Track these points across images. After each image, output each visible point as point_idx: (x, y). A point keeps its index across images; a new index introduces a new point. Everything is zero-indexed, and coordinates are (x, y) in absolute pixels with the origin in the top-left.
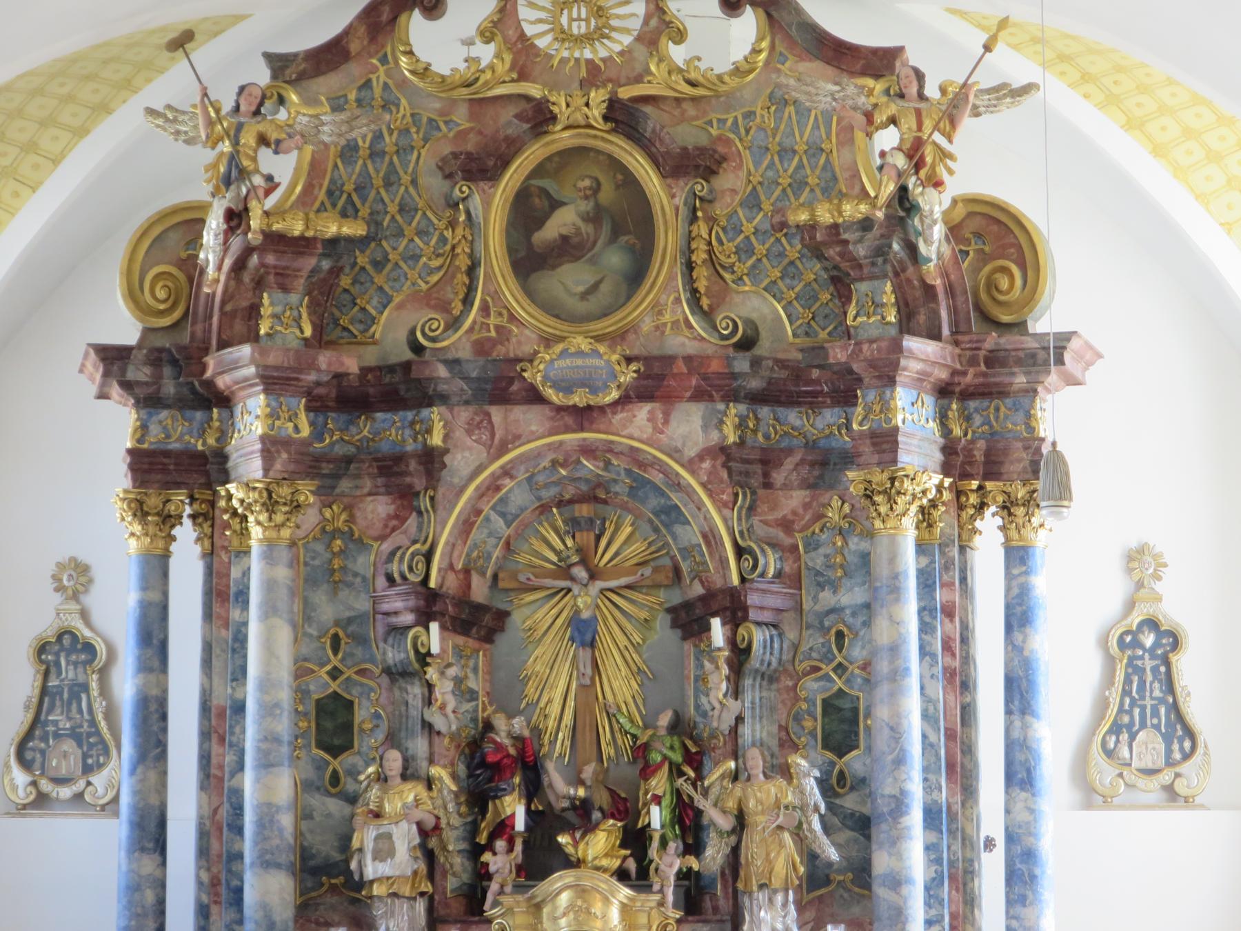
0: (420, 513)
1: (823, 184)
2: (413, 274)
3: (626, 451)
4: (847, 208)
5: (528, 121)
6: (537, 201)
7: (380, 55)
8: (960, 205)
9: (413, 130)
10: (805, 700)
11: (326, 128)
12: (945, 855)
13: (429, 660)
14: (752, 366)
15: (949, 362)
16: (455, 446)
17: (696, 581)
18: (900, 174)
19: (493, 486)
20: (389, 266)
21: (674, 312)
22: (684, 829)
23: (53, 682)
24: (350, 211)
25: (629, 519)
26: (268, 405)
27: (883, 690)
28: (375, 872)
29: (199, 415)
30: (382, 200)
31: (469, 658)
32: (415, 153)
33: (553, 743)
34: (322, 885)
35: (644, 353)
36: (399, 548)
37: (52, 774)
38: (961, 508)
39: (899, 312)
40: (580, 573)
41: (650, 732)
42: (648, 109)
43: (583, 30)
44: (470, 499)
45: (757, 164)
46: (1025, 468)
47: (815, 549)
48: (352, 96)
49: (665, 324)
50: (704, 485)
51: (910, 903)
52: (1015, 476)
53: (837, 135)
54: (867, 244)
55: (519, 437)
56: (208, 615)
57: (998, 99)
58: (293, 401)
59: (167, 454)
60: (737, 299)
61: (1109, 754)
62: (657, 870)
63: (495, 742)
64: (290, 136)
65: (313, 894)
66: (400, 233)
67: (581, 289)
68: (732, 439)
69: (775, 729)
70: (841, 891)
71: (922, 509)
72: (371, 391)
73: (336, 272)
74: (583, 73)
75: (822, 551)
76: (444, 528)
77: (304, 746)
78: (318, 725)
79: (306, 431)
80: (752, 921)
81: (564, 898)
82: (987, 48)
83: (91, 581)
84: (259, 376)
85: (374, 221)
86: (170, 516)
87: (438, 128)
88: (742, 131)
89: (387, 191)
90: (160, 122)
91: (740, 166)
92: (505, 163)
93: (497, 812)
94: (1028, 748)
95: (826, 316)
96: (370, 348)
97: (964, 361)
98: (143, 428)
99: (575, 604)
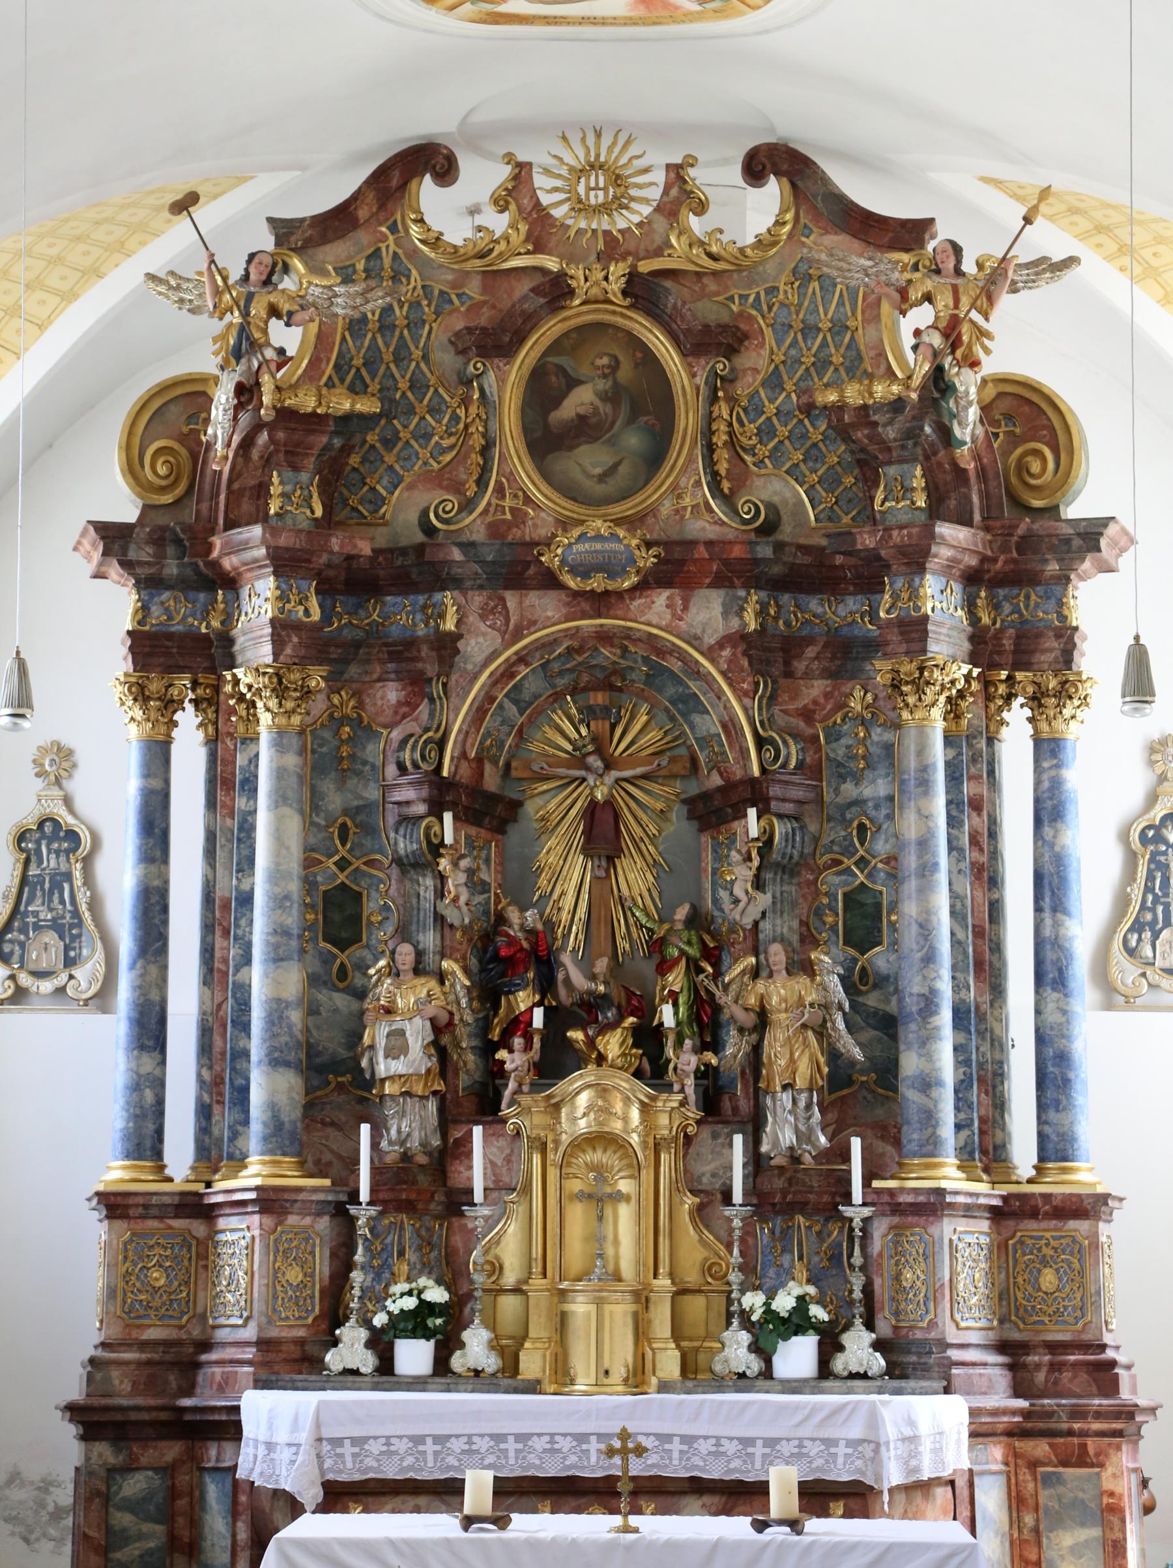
0: (432, 700)
1: (847, 363)
2: (424, 453)
3: (644, 637)
4: (879, 389)
5: (544, 296)
6: (554, 379)
7: (390, 222)
8: (990, 385)
9: (425, 302)
10: (826, 894)
11: (339, 300)
12: (974, 1057)
13: (442, 851)
14: (775, 552)
15: (980, 548)
16: (469, 631)
17: (715, 772)
18: (936, 354)
19: (508, 672)
20: (400, 445)
21: (694, 495)
22: (702, 1027)
23: (33, 871)
24: (359, 386)
25: (645, 708)
26: (278, 588)
27: (911, 886)
28: (387, 1069)
29: (202, 596)
30: (393, 376)
31: (481, 849)
32: (427, 328)
33: (566, 936)
34: (329, 1083)
35: (664, 537)
36: (411, 735)
37: (32, 967)
38: (989, 698)
39: (928, 497)
40: (595, 762)
41: (666, 926)
42: (668, 284)
43: (601, 199)
44: (483, 686)
45: (779, 343)
46: (1056, 658)
47: (837, 740)
48: (360, 266)
49: (685, 508)
50: (723, 674)
51: (941, 1106)
52: (1046, 666)
53: (863, 312)
54: (896, 426)
55: (534, 623)
56: (211, 803)
57: (1037, 274)
58: (304, 584)
59: (170, 636)
60: (758, 482)
61: (1131, 952)
62: (675, 1069)
63: (508, 935)
64: (302, 308)
65: (319, 1093)
66: (411, 411)
67: (598, 471)
68: (752, 626)
69: (795, 924)
70: (864, 1092)
71: (949, 699)
72: (382, 573)
73: (347, 450)
74: (601, 245)
75: (843, 741)
76: (457, 716)
77: (311, 939)
78: (325, 917)
79: (316, 615)
80: (775, 1121)
81: (583, 1099)
82: (1028, 220)
83: (74, 766)
84: (269, 555)
85: (385, 394)
86: (173, 701)
87: (451, 302)
88: (765, 307)
89: (397, 366)
90: (162, 288)
91: (762, 344)
92: (520, 338)
93: (510, 1008)
94: (1060, 947)
95: (850, 501)
96: (380, 529)
97: (995, 546)
98: (144, 610)
99: (592, 794)
